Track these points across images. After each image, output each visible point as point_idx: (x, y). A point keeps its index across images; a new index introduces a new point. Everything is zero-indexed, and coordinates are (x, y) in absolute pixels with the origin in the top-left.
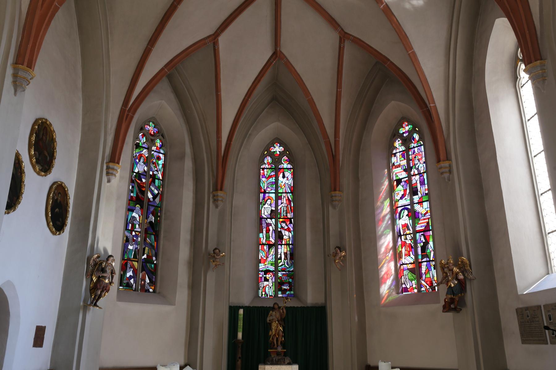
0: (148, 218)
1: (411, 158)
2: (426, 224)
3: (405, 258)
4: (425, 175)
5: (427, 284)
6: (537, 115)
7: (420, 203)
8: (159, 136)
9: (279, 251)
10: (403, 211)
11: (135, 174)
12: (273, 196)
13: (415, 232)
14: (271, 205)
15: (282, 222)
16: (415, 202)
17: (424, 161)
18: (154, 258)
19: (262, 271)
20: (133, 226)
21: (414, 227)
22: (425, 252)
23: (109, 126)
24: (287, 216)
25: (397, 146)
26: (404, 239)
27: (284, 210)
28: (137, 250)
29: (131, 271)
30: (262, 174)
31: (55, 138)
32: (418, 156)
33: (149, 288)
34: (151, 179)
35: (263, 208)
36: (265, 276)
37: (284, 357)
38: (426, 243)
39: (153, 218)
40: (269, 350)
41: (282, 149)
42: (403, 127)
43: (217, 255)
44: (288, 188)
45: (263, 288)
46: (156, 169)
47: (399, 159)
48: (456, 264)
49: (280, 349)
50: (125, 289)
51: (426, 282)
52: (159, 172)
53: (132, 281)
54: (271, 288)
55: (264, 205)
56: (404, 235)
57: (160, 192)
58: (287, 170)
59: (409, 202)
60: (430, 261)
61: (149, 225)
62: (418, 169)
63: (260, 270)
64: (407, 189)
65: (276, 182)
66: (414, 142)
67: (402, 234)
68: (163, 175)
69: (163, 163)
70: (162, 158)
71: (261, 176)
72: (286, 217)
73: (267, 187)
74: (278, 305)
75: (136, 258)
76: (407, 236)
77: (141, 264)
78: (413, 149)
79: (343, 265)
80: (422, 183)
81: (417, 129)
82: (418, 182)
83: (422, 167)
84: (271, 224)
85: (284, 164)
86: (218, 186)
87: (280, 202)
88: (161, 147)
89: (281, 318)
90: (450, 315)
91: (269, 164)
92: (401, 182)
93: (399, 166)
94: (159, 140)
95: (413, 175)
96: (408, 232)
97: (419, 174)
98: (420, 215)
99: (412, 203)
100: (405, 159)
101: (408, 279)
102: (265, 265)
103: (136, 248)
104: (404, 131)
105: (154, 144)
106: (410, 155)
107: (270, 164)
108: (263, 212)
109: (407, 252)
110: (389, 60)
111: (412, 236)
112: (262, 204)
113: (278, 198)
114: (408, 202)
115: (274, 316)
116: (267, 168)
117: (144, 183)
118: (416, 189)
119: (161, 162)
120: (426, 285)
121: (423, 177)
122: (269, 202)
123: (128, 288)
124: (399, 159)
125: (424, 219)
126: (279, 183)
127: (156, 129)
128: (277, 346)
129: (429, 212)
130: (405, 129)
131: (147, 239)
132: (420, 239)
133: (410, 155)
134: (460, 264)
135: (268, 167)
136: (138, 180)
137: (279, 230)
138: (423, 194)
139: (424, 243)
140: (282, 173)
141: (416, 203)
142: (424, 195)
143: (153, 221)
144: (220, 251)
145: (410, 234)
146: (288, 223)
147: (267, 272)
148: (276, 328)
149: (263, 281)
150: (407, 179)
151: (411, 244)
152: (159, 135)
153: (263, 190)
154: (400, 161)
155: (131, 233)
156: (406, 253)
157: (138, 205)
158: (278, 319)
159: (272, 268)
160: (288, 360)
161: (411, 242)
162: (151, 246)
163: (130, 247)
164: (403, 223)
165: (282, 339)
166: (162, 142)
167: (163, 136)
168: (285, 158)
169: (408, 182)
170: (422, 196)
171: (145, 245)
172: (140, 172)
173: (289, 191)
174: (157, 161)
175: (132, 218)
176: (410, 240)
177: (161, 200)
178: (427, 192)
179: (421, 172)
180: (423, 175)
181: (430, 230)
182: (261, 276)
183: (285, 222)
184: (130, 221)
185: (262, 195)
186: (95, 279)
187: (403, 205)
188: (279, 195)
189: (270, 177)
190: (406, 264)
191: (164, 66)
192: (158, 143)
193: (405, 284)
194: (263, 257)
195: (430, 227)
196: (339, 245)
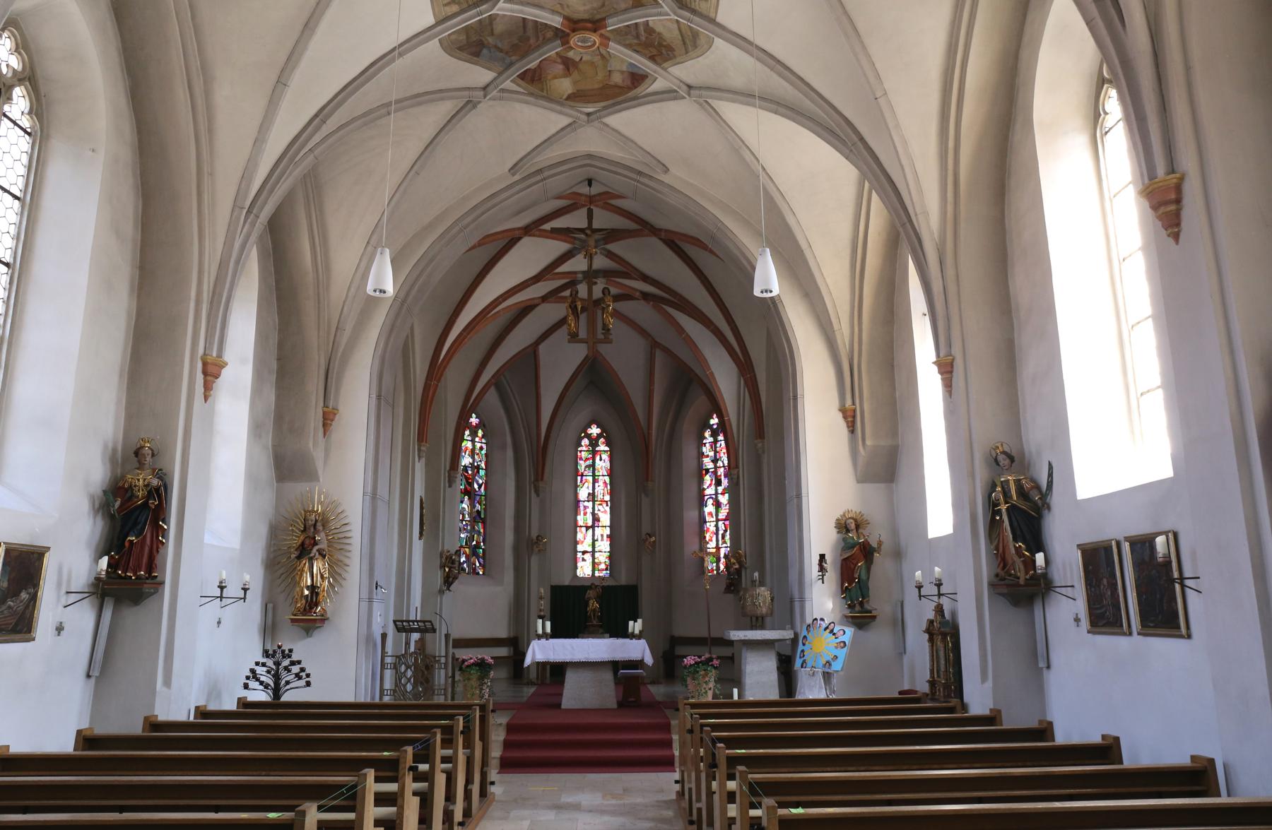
6: (1121, 122)
7: (723, 494)
12: (590, 479)
13: (718, 520)
15: (599, 504)
18: (482, 544)
20: (463, 515)
21: (717, 515)
34: (476, 470)
38: (726, 531)
41: (599, 431)
53: (465, 565)
65: (593, 465)
68: (486, 465)
82: (723, 474)
86: (539, 474)
87: (597, 484)
88: (483, 437)
90: (731, 596)
91: (586, 446)
93: (708, 456)
96: (712, 519)
97: (724, 466)
99: (716, 494)
103: (467, 536)
113: (595, 481)
114: (713, 492)
115: (590, 593)
117: (470, 475)
119: (484, 452)
122: (586, 484)
127: (477, 420)
146: (605, 505)
147: (584, 553)
148: (594, 605)
150: (713, 470)
163: (462, 536)
167: (484, 426)
168: (602, 440)
177: (485, 489)
186: (447, 570)
189: (587, 459)
192: (480, 433)
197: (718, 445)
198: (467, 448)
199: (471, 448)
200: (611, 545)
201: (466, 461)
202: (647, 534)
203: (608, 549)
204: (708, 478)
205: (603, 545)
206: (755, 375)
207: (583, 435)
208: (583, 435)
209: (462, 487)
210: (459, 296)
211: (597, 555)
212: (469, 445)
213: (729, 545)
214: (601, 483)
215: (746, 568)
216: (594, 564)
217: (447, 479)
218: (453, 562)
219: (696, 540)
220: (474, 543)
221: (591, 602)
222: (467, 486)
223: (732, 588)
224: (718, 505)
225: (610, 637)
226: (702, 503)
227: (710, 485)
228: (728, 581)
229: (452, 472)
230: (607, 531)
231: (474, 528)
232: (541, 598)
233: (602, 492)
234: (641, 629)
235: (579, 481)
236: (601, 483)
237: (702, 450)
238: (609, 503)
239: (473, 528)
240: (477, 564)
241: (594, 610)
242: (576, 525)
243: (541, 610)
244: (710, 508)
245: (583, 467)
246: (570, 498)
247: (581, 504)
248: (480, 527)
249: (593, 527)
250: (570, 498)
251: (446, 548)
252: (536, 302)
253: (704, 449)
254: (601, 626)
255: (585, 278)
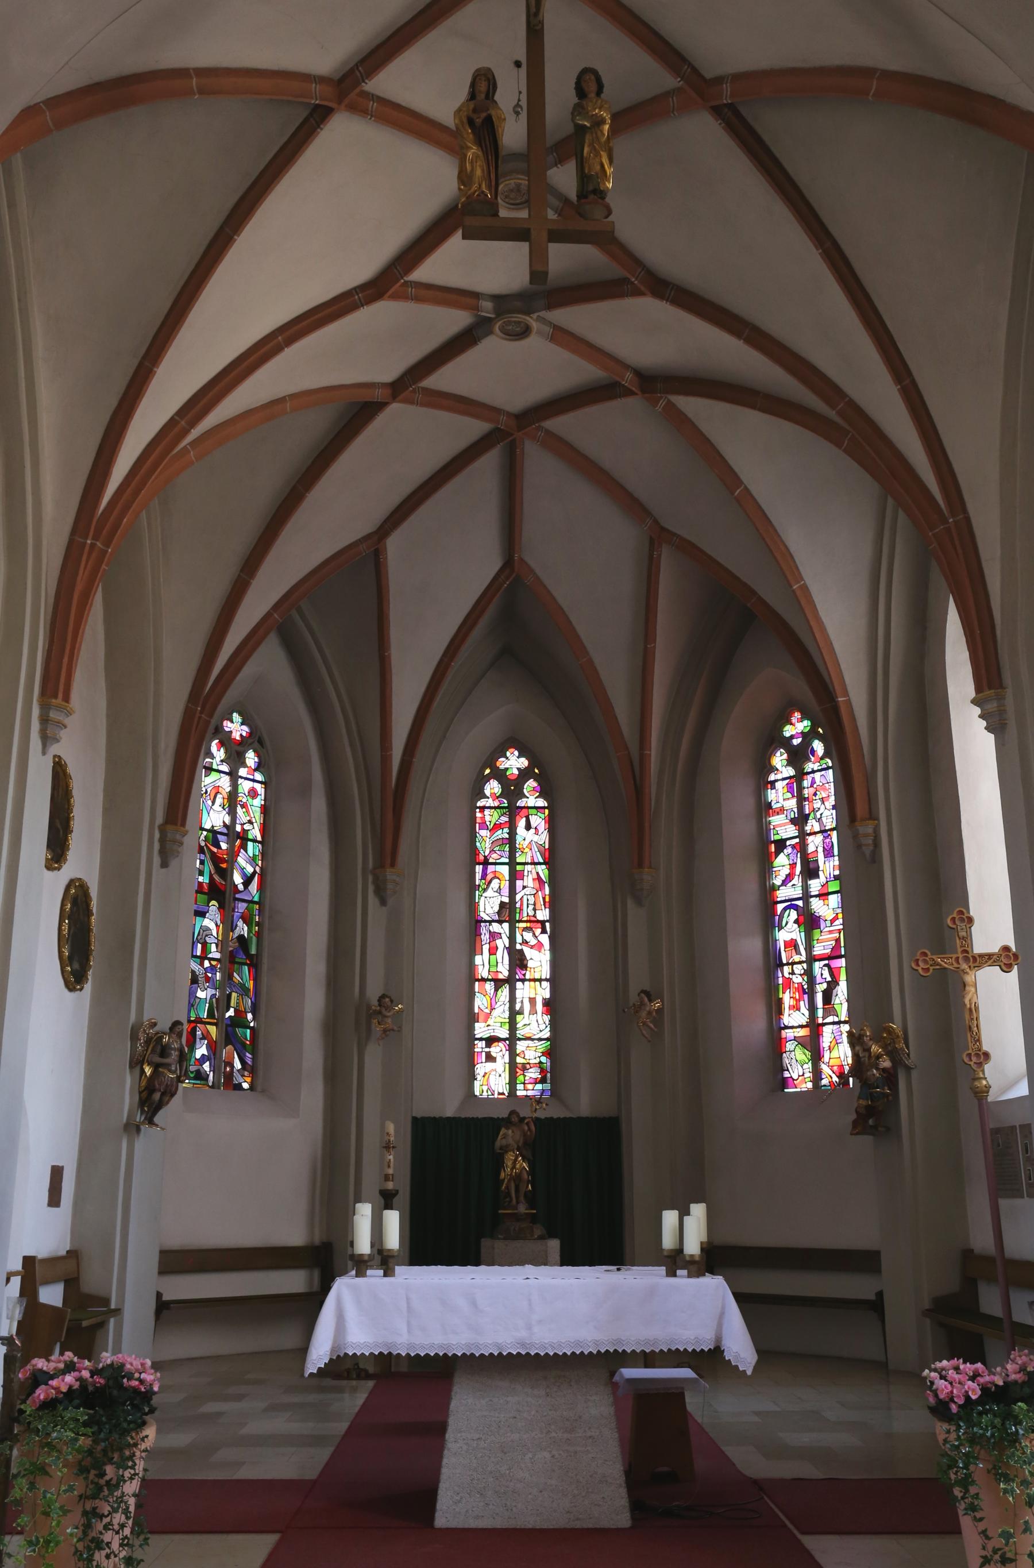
0: (236, 928)
1: (806, 796)
2: (833, 943)
3: (789, 1015)
4: (834, 834)
5: (834, 1072)
7: (823, 895)
8: (253, 742)
9: (519, 994)
10: (788, 911)
11: (205, 833)
12: (505, 870)
13: (811, 959)
14: (499, 891)
15: (525, 929)
16: (812, 894)
17: (833, 803)
18: (250, 1016)
19: (481, 1039)
20: (205, 945)
21: (809, 948)
22: (830, 1004)
23: (162, 745)
24: (534, 916)
25: (779, 766)
26: (789, 973)
27: (530, 902)
28: (214, 1000)
29: (205, 1046)
30: (478, 821)
31: (71, 790)
32: (822, 792)
33: (241, 1080)
34: (238, 842)
35: (482, 898)
36: (487, 1050)
37: (531, 1225)
38: (833, 984)
39: (246, 928)
40: (500, 1212)
41: (524, 762)
42: (791, 724)
43: (386, 1010)
44: (538, 853)
45: (484, 1076)
46: (248, 818)
47: (780, 794)
48: (877, 1039)
49: (522, 1209)
50: (194, 1084)
51: (832, 1066)
52: (255, 824)
53: (206, 1066)
54: (500, 1076)
55: (485, 890)
56: (788, 964)
57: (258, 869)
58: (534, 811)
59: (801, 892)
60: (839, 1023)
61: (237, 944)
62: (819, 820)
63: (476, 1037)
64: (796, 863)
65: (511, 840)
66: (813, 759)
67: (784, 961)
68: (264, 830)
69: (263, 802)
70: (259, 793)
71: (477, 825)
72: (533, 919)
73: (492, 851)
74: (518, 1115)
75: (213, 1017)
76: (795, 966)
77: (224, 1030)
78: (812, 775)
79: (656, 1030)
80: (828, 853)
81: (821, 732)
82: (820, 850)
83: (829, 819)
84: (500, 934)
85: (528, 798)
89: (525, 1143)
90: (868, 1139)
91: (495, 797)
92: (785, 847)
93: (782, 810)
94: (253, 753)
95: (810, 834)
96: (797, 958)
98: (822, 922)
99: (806, 896)
100: (793, 796)
101: (794, 1061)
102: (488, 1026)
103: (213, 996)
104: (794, 733)
105: (244, 764)
106: (804, 788)
107: (498, 797)
108: (481, 908)
109: (795, 1002)
110: (753, 593)
111: (805, 968)
112: (480, 889)
113: (515, 876)
114: (798, 892)
115: (508, 1136)
116: (490, 808)
118: (816, 865)
119: (258, 802)
120: (831, 1073)
121: (831, 839)
122: (495, 884)
123: (198, 1082)
124: (780, 794)
125: (831, 932)
126: (517, 842)
127: (245, 728)
128: (518, 1202)
129: (840, 916)
130: (796, 727)
131: (235, 974)
132: (822, 974)
133: (804, 788)
134: (885, 1037)
135: (492, 805)
136: (212, 845)
137: (518, 947)
138: (828, 877)
139: (828, 982)
140: (524, 819)
141: (816, 896)
142: (831, 879)
143: (246, 935)
144: (392, 1001)
145: (800, 963)
146: (538, 931)
147: (491, 1041)
148: (516, 1164)
149: (484, 1060)
150: (797, 840)
151: (803, 984)
152: (252, 740)
153: (481, 858)
154: (784, 800)
155: (202, 964)
156: (791, 1004)
157: (213, 902)
158: (518, 1146)
159: (504, 1033)
160: (538, 1230)
161: (803, 979)
162: (243, 990)
163: (201, 994)
164: (788, 939)
165: (527, 1186)
166: (259, 756)
167: (260, 742)
168: (531, 784)
169: (798, 847)
170: (827, 882)
171: (230, 988)
172: (215, 828)
173: (541, 861)
174: (250, 800)
175: (201, 931)
176: (801, 975)
177: (261, 887)
178: (837, 872)
179: (827, 828)
180: (829, 835)
181: (840, 957)
182: (480, 1050)
183: (532, 928)
184: (199, 938)
185: (479, 869)
186: (148, 1071)
187: (787, 898)
188: (519, 868)
189: (497, 827)
190: (792, 1027)
191: (271, 609)
193: (788, 1070)
194: (482, 1007)
195: (843, 949)
196: (647, 988)
197: (806, 783)
198: (217, 790)
199: (228, 789)
200: (553, 1024)
201: (215, 817)
202: (644, 992)
203: (546, 1034)
204: (782, 863)
205: (534, 1024)
206: (968, 520)
207: (488, 771)
208: (488, 771)
209: (204, 879)
210: (163, 304)
211: (521, 1046)
212: (225, 783)
213: (844, 1017)
214: (529, 881)
215: (908, 1069)
216: (514, 1069)
217: (157, 846)
218: (164, 1051)
219: (760, 1009)
220: (231, 1013)
221: (510, 1157)
222: (216, 878)
223: (871, 1122)
224: (810, 922)
225: (569, 1259)
226: (770, 922)
227: (789, 878)
228: (863, 1102)
229: (169, 828)
230: (544, 991)
231: (230, 977)
232: (388, 1147)
233: (532, 900)
234: (705, 1239)
235: (478, 876)
236: (529, 881)
237: (766, 796)
238: (548, 925)
239: (228, 977)
240: (238, 1065)
241: (517, 1178)
242: (472, 978)
243: (387, 1178)
244: (789, 931)
245: (488, 845)
246: (458, 912)
247: (484, 929)
248: (244, 976)
249: (511, 981)
250: (458, 912)
251: (146, 1017)
252: (378, 395)
253: (771, 795)
254: (533, 1219)
255: (499, 313)
